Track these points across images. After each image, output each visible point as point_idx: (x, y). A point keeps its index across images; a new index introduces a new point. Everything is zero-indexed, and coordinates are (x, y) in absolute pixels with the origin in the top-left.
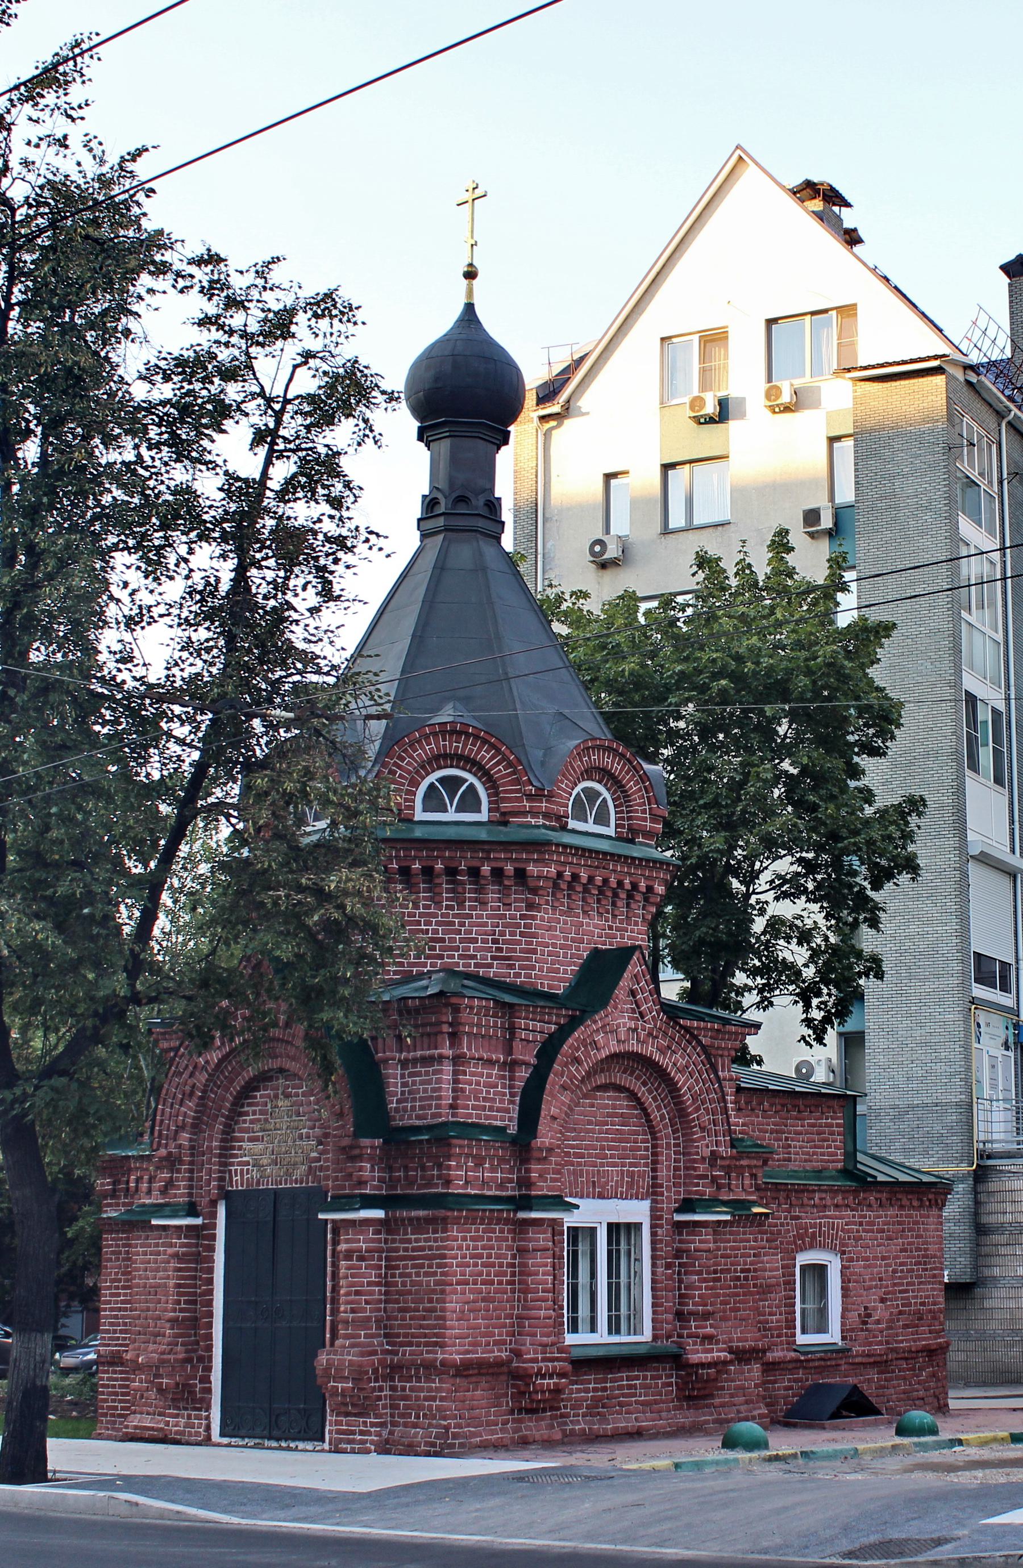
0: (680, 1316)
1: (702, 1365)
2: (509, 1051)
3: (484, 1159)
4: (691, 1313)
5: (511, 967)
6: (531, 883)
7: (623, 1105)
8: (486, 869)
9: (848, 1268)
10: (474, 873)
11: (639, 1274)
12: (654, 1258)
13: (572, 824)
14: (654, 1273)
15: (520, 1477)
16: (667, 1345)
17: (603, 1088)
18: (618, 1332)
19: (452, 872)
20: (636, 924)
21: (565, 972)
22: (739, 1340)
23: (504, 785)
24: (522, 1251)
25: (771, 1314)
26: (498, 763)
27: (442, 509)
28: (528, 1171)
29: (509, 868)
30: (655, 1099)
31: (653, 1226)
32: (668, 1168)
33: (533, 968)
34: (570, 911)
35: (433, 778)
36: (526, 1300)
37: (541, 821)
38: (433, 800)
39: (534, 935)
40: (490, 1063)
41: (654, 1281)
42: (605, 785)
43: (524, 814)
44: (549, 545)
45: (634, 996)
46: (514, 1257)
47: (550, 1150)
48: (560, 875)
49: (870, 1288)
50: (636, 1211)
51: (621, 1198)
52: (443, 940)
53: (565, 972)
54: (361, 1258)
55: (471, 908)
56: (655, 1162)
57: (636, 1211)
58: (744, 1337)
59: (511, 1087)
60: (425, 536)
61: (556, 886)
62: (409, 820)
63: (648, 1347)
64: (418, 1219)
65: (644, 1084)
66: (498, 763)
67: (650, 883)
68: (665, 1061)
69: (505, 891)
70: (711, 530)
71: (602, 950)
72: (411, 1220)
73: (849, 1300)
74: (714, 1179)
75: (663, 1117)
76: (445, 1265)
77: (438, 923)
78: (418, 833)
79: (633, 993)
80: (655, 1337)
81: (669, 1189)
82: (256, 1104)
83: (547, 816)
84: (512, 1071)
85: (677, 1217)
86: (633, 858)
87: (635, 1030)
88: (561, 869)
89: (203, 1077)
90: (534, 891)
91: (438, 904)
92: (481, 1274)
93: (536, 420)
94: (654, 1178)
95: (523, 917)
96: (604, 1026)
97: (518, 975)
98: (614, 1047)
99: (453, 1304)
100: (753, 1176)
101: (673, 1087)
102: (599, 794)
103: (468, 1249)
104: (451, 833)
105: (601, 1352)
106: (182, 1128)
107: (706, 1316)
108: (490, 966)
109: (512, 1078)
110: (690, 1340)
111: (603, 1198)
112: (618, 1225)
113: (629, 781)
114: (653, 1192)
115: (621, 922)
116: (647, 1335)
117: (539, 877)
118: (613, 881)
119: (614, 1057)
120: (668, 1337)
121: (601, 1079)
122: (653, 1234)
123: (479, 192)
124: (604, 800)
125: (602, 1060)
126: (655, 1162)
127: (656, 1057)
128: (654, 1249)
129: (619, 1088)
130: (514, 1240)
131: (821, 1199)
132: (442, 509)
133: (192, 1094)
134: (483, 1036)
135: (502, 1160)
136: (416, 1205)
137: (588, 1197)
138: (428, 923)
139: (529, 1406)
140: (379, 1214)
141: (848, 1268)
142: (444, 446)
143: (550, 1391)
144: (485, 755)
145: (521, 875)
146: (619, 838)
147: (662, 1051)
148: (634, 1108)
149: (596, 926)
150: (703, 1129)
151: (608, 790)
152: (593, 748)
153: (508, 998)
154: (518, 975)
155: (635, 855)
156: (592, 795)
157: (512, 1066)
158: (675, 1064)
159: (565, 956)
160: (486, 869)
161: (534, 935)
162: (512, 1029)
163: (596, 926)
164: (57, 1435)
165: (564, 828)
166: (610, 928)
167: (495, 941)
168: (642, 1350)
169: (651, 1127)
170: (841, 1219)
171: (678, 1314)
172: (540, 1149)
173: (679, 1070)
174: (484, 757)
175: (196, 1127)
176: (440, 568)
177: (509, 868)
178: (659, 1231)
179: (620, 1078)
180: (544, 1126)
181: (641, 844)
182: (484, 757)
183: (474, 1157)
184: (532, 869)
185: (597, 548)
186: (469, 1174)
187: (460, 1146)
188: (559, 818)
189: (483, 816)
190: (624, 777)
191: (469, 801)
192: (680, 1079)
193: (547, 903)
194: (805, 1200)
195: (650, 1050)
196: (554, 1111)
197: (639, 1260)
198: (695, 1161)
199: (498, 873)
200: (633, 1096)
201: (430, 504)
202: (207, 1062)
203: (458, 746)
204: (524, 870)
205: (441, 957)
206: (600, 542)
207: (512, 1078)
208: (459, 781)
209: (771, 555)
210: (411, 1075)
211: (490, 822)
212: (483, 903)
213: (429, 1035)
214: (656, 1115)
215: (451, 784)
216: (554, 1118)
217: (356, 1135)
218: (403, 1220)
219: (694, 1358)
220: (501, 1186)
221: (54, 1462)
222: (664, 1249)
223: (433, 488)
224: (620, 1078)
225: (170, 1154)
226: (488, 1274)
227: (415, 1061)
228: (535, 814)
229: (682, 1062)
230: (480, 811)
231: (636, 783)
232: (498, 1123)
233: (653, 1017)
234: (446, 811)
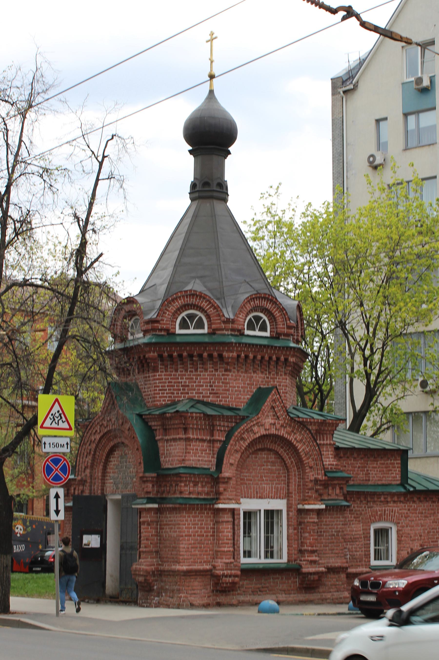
0: (301, 552)
1: (311, 574)
2: (212, 435)
3: (198, 482)
4: (306, 550)
5: (218, 397)
6: (226, 361)
7: (272, 457)
8: (205, 354)
9: (401, 530)
10: (200, 356)
11: (281, 532)
12: (288, 525)
13: (247, 332)
14: (288, 532)
15: (182, 617)
16: (293, 564)
17: (262, 450)
18: (272, 557)
19: (191, 356)
20: (281, 375)
21: (244, 398)
22: (333, 563)
23: (213, 317)
24: (218, 522)
25: (356, 551)
26: (210, 308)
27: (197, 189)
28: (219, 487)
29: (215, 354)
30: (288, 454)
31: (288, 511)
32: (295, 485)
33: (228, 397)
34: (246, 372)
35: (184, 314)
36: (219, 543)
37: (230, 332)
38: (184, 325)
39: (227, 383)
40: (203, 440)
41: (288, 536)
42: (264, 314)
43: (222, 330)
44: (350, 157)
45: (274, 409)
46: (214, 525)
47: (229, 479)
48: (239, 356)
49: (415, 540)
50: (279, 504)
51: (272, 498)
52: (188, 386)
53: (244, 398)
54: (148, 524)
55: (200, 372)
56: (288, 483)
57: (279, 504)
58: (336, 562)
59: (213, 451)
60: (192, 199)
61: (238, 360)
62: (174, 334)
63: (286, 565)
64: (170, 508)
65: (282, 447)
66: (210, 308)
67: (286, 357)
68: (291, 438)
69: (215, 364)
70: (427, 147)
71: (263, 389)
72: (168, 508)
73: (402, 545)
74: (317, 491)
75: (292, 462)
76: (180, 528)
77: (186, 379)
78: (178, 339)
79: (273, 408)
80: (289, 561)
81: (295, 495)
82: (115, 457)
83: (233, 330)
84: (213, 444)
85: (300, 506)
86: (276, 347)
87: (274, 424)
88: (239, 353)
89: (94, 446)
90: (227, 364)
91: (186, 371)
92: (197, 532)
93: (342, 93)
94: (288, 489)
95: (223, 375)
96: (257, 423)
97: (221, 401)
98: (263, 432)
99: (183, 545)
100: (341, 488)
101: (296, 450)
102: (261, 318)
103: (191, 521)
104: (192, 339)
105: (261, 566)
106: (86, 468)
107: (313, 552)
108: (209, 397)
109: (213, 447)
110: (304, 562)
111: (262, 498)
112: (272, 511)
113: (275, 311)
114: (288, 496)
115: (274, 375)
116: (285, 559)
117: (228, 358)
118: (267, 358)
119: (263, 437)
120: (295, 560)
121: (259, 446)
122: (288, 515)
123: (214, 36)
124: (264, 321)
125: (256, 438)
126: (288, 483)
127: (286, 436)
128: (288, 521)
129: (270, 450)
130: (214, 517)
131: (385, 498)
132: (197, 189)
133: (90, 453)
134: (200, 429)
135: (207, 483)
136: (165, 504)
137: (254, 498)
138: (182, 379)
139: (220, 589)
140: (156, 506)
141: (401, 530)
142: (200, 158)
143: (230, 583)
144: (204, 304)
145: (221, 356)
146: (272, 337)
147: (289, 434)
148: (279, 458)
149: (259, 377)
150: (311, 468)
151: (266, 316)
152: (256, 298)
153: (210, 412)
154: (221, 401)
155: (276, 345)
156: (258, 319)
157: (212, 442)
158: (295, 439)
159: (244, 391)
160: (205, 354)
161: (227, 383)
162: (213, 425)
163: (259, 377)
164: (13, 596)
165: (242, 334)
166: (268, 378)
167: (211, 386)
168: (283, 566)
169: (286, 467)
170: (397, 508)
171: (298, 549)
172: (224, 478)
173: (297, 442)
174: (204, 305)
175: (92, 467)
176: (195, 216)
177: (215, 354)
178: (291, 513)
179: (269, 445)
180: (225, 467)
181: (282, 339)
182: (204, 305)
183: (193, 482)
184: (225, 354)
185: (371, 159)
186: (188, 490)
187: (186, 477)
188: (239, 331)
189: (206, 331)
190: (273, 310)
191: (200, 325)
192: (299, 446)
193: (234, 368)
194: (376, 499)
195: (282, 432)
196: (231, 461)
197: (281, 526)
198: (307, 482)
199: (211, 356)
200: (276, 453)
201: (193, 186)
202: (95, 439)
203: (193, 301)
204: (222, 355)
205: (188, 393)
206: (372, 156)
207: (213, 447)
208: (195, 316)
209: (298, 222)
210: (169, 446)
211: (209, 334)
212: (206, 370)
213: (176, 429)
214: (288, 461)
215: (191, 317)
216: (232, 464)
217: (145, 472)
218: (165, 508)
219: (305, 570)
220: (208, 494)
221: (13, 607)
222: (294, 522)
223: (195, 178)
224: (269, 445)
225: (82, 478)
226: (201, 532)
227: (171, 440)
228: (227, 330)
229: (299, 438)
230: (203, 328)
231: (279, 312)
232: (206, 467)
233: (284, 418)
234: (189, 328)
